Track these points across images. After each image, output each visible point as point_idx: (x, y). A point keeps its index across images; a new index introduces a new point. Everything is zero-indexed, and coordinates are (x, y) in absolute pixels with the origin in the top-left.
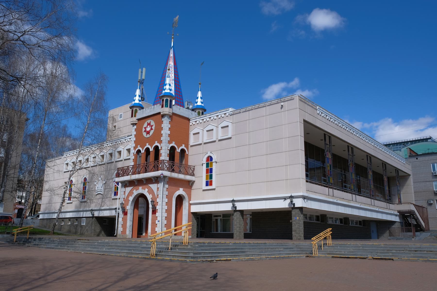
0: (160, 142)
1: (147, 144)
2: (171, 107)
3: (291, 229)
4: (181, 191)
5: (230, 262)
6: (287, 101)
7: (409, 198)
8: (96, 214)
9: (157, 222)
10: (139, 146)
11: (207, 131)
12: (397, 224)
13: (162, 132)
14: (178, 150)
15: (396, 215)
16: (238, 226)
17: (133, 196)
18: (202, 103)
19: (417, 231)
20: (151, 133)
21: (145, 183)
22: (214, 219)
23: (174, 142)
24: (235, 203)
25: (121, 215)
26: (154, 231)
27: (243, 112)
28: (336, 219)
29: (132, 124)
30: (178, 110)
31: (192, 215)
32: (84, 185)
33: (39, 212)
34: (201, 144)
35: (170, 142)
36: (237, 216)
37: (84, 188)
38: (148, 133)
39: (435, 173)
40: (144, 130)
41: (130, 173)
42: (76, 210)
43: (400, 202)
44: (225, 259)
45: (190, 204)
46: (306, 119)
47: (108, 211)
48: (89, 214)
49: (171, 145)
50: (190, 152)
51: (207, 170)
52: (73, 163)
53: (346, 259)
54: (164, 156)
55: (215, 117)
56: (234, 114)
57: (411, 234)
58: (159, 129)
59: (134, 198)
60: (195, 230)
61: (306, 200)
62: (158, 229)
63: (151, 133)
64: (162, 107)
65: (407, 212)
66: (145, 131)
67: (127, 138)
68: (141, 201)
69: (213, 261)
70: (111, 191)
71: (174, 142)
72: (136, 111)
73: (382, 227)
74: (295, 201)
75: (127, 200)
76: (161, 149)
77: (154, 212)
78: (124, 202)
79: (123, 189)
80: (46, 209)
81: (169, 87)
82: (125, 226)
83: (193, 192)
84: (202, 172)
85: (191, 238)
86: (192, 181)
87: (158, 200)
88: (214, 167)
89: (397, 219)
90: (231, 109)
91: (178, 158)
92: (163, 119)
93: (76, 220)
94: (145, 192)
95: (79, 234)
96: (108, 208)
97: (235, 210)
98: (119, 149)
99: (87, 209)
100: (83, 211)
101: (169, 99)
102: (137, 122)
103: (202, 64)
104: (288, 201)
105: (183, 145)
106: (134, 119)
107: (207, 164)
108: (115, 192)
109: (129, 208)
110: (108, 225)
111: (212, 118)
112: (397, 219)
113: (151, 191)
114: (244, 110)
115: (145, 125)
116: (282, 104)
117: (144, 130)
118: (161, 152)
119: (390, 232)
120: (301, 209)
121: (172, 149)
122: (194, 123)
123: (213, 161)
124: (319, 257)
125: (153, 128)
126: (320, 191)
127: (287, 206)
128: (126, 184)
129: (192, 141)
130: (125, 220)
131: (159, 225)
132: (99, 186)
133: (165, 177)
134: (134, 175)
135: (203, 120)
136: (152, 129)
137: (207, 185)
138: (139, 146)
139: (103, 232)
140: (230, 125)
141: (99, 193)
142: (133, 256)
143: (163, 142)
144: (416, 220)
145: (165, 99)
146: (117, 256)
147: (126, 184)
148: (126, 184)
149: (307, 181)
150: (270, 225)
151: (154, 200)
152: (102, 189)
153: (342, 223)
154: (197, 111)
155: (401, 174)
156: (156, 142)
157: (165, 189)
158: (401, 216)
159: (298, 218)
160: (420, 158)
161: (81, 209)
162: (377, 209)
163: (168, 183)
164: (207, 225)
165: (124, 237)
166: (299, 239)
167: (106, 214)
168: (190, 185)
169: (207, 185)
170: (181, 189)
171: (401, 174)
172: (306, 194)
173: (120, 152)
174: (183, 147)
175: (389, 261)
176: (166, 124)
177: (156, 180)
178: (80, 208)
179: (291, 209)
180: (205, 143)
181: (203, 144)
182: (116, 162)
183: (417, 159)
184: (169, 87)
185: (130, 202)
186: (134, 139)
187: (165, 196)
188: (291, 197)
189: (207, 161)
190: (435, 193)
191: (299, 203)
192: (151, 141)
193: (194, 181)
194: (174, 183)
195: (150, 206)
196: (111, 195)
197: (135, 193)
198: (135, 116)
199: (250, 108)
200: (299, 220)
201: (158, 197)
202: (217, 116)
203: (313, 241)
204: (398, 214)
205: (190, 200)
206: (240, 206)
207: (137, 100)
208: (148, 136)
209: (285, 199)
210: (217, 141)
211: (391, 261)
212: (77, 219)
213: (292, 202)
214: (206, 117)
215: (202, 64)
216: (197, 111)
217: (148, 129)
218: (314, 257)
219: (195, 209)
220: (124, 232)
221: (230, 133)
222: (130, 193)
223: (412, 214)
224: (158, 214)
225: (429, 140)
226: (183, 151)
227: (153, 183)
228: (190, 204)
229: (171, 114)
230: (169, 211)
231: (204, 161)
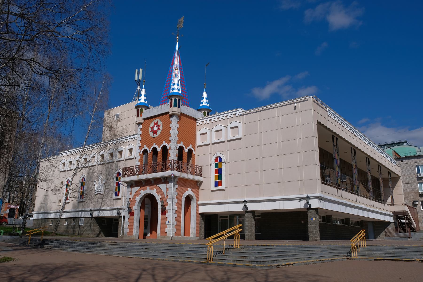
0: (169, 142)
1: (154, 144)
2: (179, 107)
3: (308, 230)
4: (189, 192)
7: (399, 199)
8: (96, 214)
9: (167, 223)
10: (145, 146)
11: (215, 131)
13: (171, 132)
14: (186, 150)
15: (391, 216)
17: (140, 196)
20: (159, 132)
21: (153, 183)
22: (220, 219)
23: (182, 142)
24: (247, 204)
25: (127, 216)
26: (164, 233)
27: (253, 113)
29: (137, 124)
31: (199, 216)
32: (82, 185)
33: (33, 212)
34: (209, 145)
35: (178, 142)
37: (82, 188)
39: (420, 175)
41: (137, 173)
42: (73, 210)
43: (393, 204)
44: (288, 263)
45: (198, 205)
46: (319, 121)
47: (109, 211)
48: (88, 215)
49: (180, 145)
50: (197, 152)
51: (216, 171)
52: (77, 161)
53: (390, 262)
54: (173, 156)
55: (224, 118)
59: (141, 198)
60: (203, 230)
61: (321, 201)
63: (159, 132)
64: (171, 106)
65: (401, 213)
66: (152, 131)
67: (129, 138)
68: (149, 203)
69: (279, 266)
70: (112, 190)
71: (182, 142)
72: (142, 111)
73: (375, 228)
74: (311, 202)
75: (133, 200)
76: (170, 149)
77: (164, 212)
78: (130, 202)
80: (40, 208)
81: (176, 86)
82: (131, 227)
83: (201, 193)
85: (199, 239)
86: (200, 181)
87: (168, 200)
88: (224, 167)
90: (240, 110)
91: (185, 157)
92: (171, 119)
93: (52, 221)
94: (154, 192)
95: (77, 234)
96: (109, 208)
97: (246, 210)
98: (120, 149)
99: (86, 209)
100: (82, 211)
101: (178, 99)
102: (143, 122)
103: (207, 65)
105: (191, 145)
106: (140, 119)
108: (116, 192)
109: (136, 208)
110: (109, 226)
111: (220, 119)
112: (391, 220)
113: (160, 192)
115: (152, 125)
117: (150, 129)
118: (170, 151)
120: (316, 209)
121: (181, 149)
122: (201, 123)
123: (223, 161)
124: (360, 259)
125: (161, 127)
126: (332, 192)
128: (131, 184)
129: (199, 141)
130: (131, 221)
131: (169, 225)
132: (97, 185)
133: (175, 177)
134: (142, 175)
135: (211, 120)
136: (159, 129)
138: (145, 146)
139: (102, 233)
140: (240, 125)
141: (99, 192)
142: (186, 260)
144: (409, 220)
145: (173, 99)
146: (165, 260)
147: (132, 184)
148: (131, 184)
151: (164, 201)
152: (102, 188)
153: (344, 224)
154: (203, 112)
155: (393, 175)
156: (164, 142)
157: (175, 190)
158: (395, 217)
159: (314, 219)
160: (405, 161)
163: (178, 183)
166: (316, 240)
167: (107, 214)
168: (198, 185)
169: (216, 185)
170: (190, 190)
171: (393, 175)
172: (322, 195)
173: (121, 152)
174: (190, 147)
176: (174, 123)
177: (166, 180)
178: (78, 207)
179: (307, 211)
180: (213, 144)
181: (211, 144)
182: (117, 161)
183: (402, 161)
184: (176, 86)
185: (137, 203)
186: (140, 139)
187: (175, 197)
188: (308, 198)
189: (215, 161)
190: (420, 195)
191: (315, 204)
192: (158, 141)
194: (183, 183)
195: (160, 206)
196: (112, 195)
197: (143, 193)
198: (141, 116)
199: (261, 108)
200: (315, 221)
201: (167, 198)
202: (226, 116)
204: (393, 214)
205: (198, 200)
206: (252, 207)
207: (143, 100)
209: (300, 199)
210: (226, 141)
212: (74, 219)
213: (308, 202)
215: (207, 65)
216: (203, 112)
217: (155, 129)
218: (352, 259)
219: (203, 210)
222: (137, 193)
223: (405, 215)
225: (405, 144)
226: (190, 151)
227: (161, 183)
230: (178, 212)
231: (213, 161)
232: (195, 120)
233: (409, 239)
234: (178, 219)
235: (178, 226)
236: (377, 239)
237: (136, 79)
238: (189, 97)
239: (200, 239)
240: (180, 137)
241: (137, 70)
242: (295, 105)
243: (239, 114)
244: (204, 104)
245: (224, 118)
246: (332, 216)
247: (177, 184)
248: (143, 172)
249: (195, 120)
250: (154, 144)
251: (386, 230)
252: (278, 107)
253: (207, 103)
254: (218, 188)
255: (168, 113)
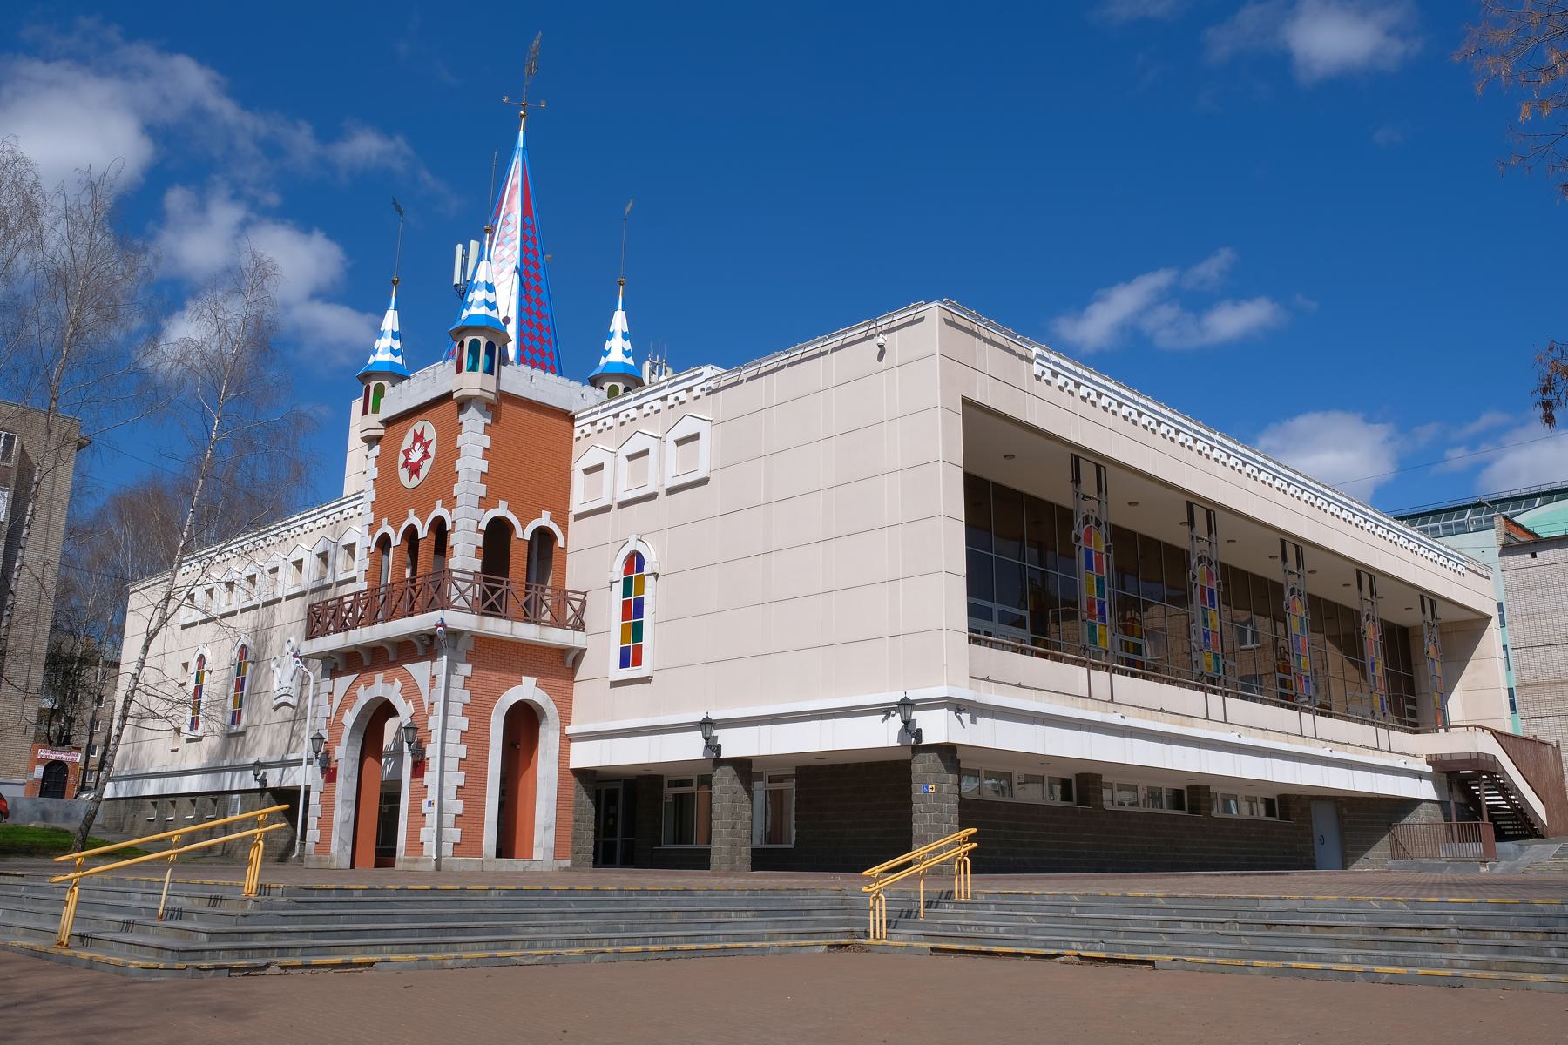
0: (451, 503)
4: (528, 689)
5: (366, 972)
6: (899, 327)
7: (1478, 709)
12: (1421, 811)
13: (459, 465)
14: (524, 533)
15: (1420, 775)
16: (732, 820)
17: (357, 708)
18: (626, 353)
19: (1501, 836)
20: (424, 471)
21: (392, 658)
22: (669, 793)
23: (503, 504)
24: (715, 733)
26: (415, 845)
28: (1251, 800)
29: (364, 439)
30: (520, 380)
31: (573, 780)
34: (607, 509)
36: (724, 782)
38: (414, 469)
40: (402, 458)
45: (567, 740)
46: (978, 397)
51: (626, 605)
54: (465, 556)
56: (718, 390)
57: (1477, 847)
58: (449, 452)
60: (589, 836)
61: (966, 717)
62: (428, 835)
64: (459, 370)
66: (406, 464)
71: (503, 504)
72: (380, 391)
74: (921, 719)
75: (335, 723)
76: (452, 531)
79: (326, 684)
83: (580, 691)
84: (607, 613)
85: (566, 869)
86: (572, 649)
88: (650, 593)
89: (1425, 790)
90: (708, 371)
91: (520, 564)
92: (462, 417)
93: (154, 804)
101: (483, 341)
102: (382, 433)
103: (398, 208)
104: (896, 722)
105: (546, 514)
107: (627, 584)
112: (1425, 790)
113: (410, 691)
114: (752, 371)
116: (880, 340)
117: (402, 458)
118: (453, 539)
119: (1396, 842)
120: (948, 753)
121: (498, 532)
122: (588, 429)
123: (647, 569)
125: (432, 450)
127: (894, 742)
129: (579, 501)
130: (327, 799)
133: (455, 634)
135: (616, 416)
137: (624, 663)
140: (704, 429)
143: (459, 503)
144: (1505, 788)
149: (973, 640)
150: (841, 812)
153: (1181, 807)
154: (607, 385)
157: (457, 681)
158: (1444, 778)
159: (932, 788)
160: (1545, 556)
161: (226, 763)
162: (1325, 753)
164: (638, 818)
165: (324, 865)
169: (624, 663)
172: (964, 692)
174: (545, 520)
175: (1137, 969)
177: (424, 646)
178: (224, 758)
179: (907, 755)
180: (622, 505)
183: (1534, 556)
185: (347, 732)
191: (936, 728)
193: (583, 651)
197: (364, 696)
198: (376, 410)
202: (664, 399)
203: (872, 879)
204: (1430, 769)
205: (566, 719)
206: (735, 744)
208: (415, 481)
209: (886, 711)
210: (662, 493)
211: (1145, 969)
214: (628, 405)
215: (398, 208)
216: (607, 385)
217: (415, 457)
219: (585, 756)
220: (324, 845)
221: (703, 460)
223: (1486, 770)
224: (431, 777)
226: (544, 538)
228: (567, 740)
229: (492, 397)
230: (473, 765)
231: (618, 572)
232: (570, 418)
233: (1483, 870)
234: (471, 793)
235: (469, 821)
236: (1355, 868)
237: (457, 280)
238: (557, 333)
239: (576, 866)
240: (495, 484)
241: (459, 247)
242: (880, 340)
243: (705, 386)
244: (380, 357)
245: (658, 405)
246: (1099, 776)
247: (467, 661)
248: (380, 616)
249: (570, 418)
250: (411, 512)
251: (1398, 830)
252: (825, 353)
253: (394, 352)
254: (631, 673)
255: (448, 396)
